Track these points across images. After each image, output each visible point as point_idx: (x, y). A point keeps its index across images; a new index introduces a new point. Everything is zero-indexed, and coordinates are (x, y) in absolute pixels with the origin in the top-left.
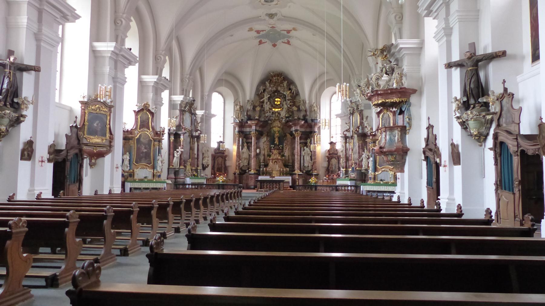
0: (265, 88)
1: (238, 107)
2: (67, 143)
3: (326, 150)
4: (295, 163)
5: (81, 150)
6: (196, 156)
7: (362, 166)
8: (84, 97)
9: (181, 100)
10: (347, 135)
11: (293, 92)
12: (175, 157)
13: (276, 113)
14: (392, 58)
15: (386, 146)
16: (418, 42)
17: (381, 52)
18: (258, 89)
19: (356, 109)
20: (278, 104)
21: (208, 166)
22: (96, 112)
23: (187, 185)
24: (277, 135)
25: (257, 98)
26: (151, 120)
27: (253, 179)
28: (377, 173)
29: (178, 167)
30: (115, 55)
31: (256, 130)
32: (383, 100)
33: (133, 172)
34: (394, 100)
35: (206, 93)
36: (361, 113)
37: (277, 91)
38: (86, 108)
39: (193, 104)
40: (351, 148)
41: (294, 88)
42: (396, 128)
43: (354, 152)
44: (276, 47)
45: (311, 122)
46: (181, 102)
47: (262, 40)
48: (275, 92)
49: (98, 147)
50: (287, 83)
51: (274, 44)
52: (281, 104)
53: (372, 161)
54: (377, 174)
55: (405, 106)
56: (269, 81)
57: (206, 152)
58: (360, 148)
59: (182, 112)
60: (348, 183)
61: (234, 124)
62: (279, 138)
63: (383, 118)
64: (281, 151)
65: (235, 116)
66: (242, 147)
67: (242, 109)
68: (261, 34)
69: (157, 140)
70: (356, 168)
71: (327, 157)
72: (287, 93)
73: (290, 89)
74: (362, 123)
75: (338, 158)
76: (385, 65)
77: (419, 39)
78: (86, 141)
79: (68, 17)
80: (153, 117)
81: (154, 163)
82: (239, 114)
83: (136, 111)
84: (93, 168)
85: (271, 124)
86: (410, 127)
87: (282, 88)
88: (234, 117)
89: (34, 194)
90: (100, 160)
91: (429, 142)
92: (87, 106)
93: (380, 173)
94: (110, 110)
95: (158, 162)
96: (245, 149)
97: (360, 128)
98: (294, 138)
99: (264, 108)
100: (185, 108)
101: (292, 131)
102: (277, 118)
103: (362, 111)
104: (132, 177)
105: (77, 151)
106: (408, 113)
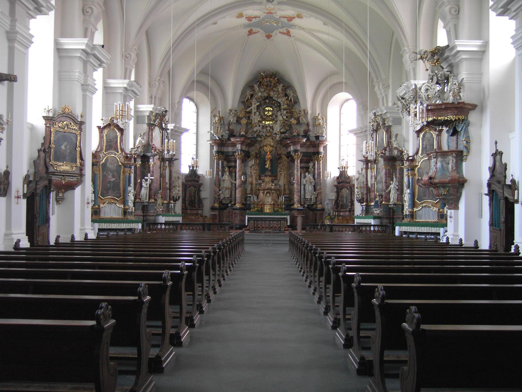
0: (253, 93)
1: (217, 119)
2: (35, 172)
3: (335, 177)
4: (293, 195)
5: (50, 181)
6: (168, 186)
7: (390, 199)
8: (49, 111)
9: (150, 111)
10: (369, 159)
11: (291, 99)
12: (143, 188)
13: (267, 127)
14: (444, 63)
15: (437, 175)
16: (480, 44)
17: (432, 55)
18: (243, 93)
19: (382, 125)
20: (269, 114)
21: (179, 198)
22: (64, 130)
23: (159, 225)
24: (269, 156)
25: (242, 106)
26: (120, 139)
27: (238, 216)
28: (415, 210)
29: (147, 200)
30: (85, 54)
31: (241, 150)
32: (435, 117)
33: (99, 208)
34: (448, 118)
35: (177, 101)
36: (388, 130)
37: (269, 97)
38: (52, 125)
39: (164, 116)
40: (374, 176)
41: (292, 94)
42: (450, 153)
43: (378, 181)
44: (271, 38)
45: (314, 139)
46: (150, 113)
47: (253, 29)
48: (266, 98)
49: (67, 177)
50: (282, 87)
51: (269, 34)
52: (273, 114)
53: (410, 194)
54: (416, 211)
55: (463, 125)
56: (259, 83)
57: (177, 180)
58: (387, 175)
59: (151, 126)
60: (372, 222)
61: (211, 142)
62: (271, 160)
63: (425, 139)
64: (273, 178)
65: (212, 132)
66: (222, 172)
67: (222, 121)
68: (253, 22)
69: (127, 166)
70: (382, 202)
71: (336, 186)
72: (282, 100)
73: (286, 95)
74: (389, 143)
75: (351, 189)
76: (436, 72)
77: (481, 40)
78: (53, 169)
79: (42, 8)
80: (122, 134)
81: (124, 196)
82: (218, 128)
83: (102, 128)
84: (60, 204)
85: (261, 141)
86: (468, 152)
87: (275, 93)
88: (211, 133)
89: (13, 239)
90: (68, 194)
91: (495, 173)
92: (53, 123)
93: (421, 209)
94: (80, 129)
95: (129, 194)
96: (226, 177)
97: (387, 149)
98: (293, 161)
99: (252, 120)
100: (155, 122)
101: (290, 152)
102: (268, 135)
103: (390, 127)
104: (98, 215)
105: (46, 182)
106: (466, 135)
